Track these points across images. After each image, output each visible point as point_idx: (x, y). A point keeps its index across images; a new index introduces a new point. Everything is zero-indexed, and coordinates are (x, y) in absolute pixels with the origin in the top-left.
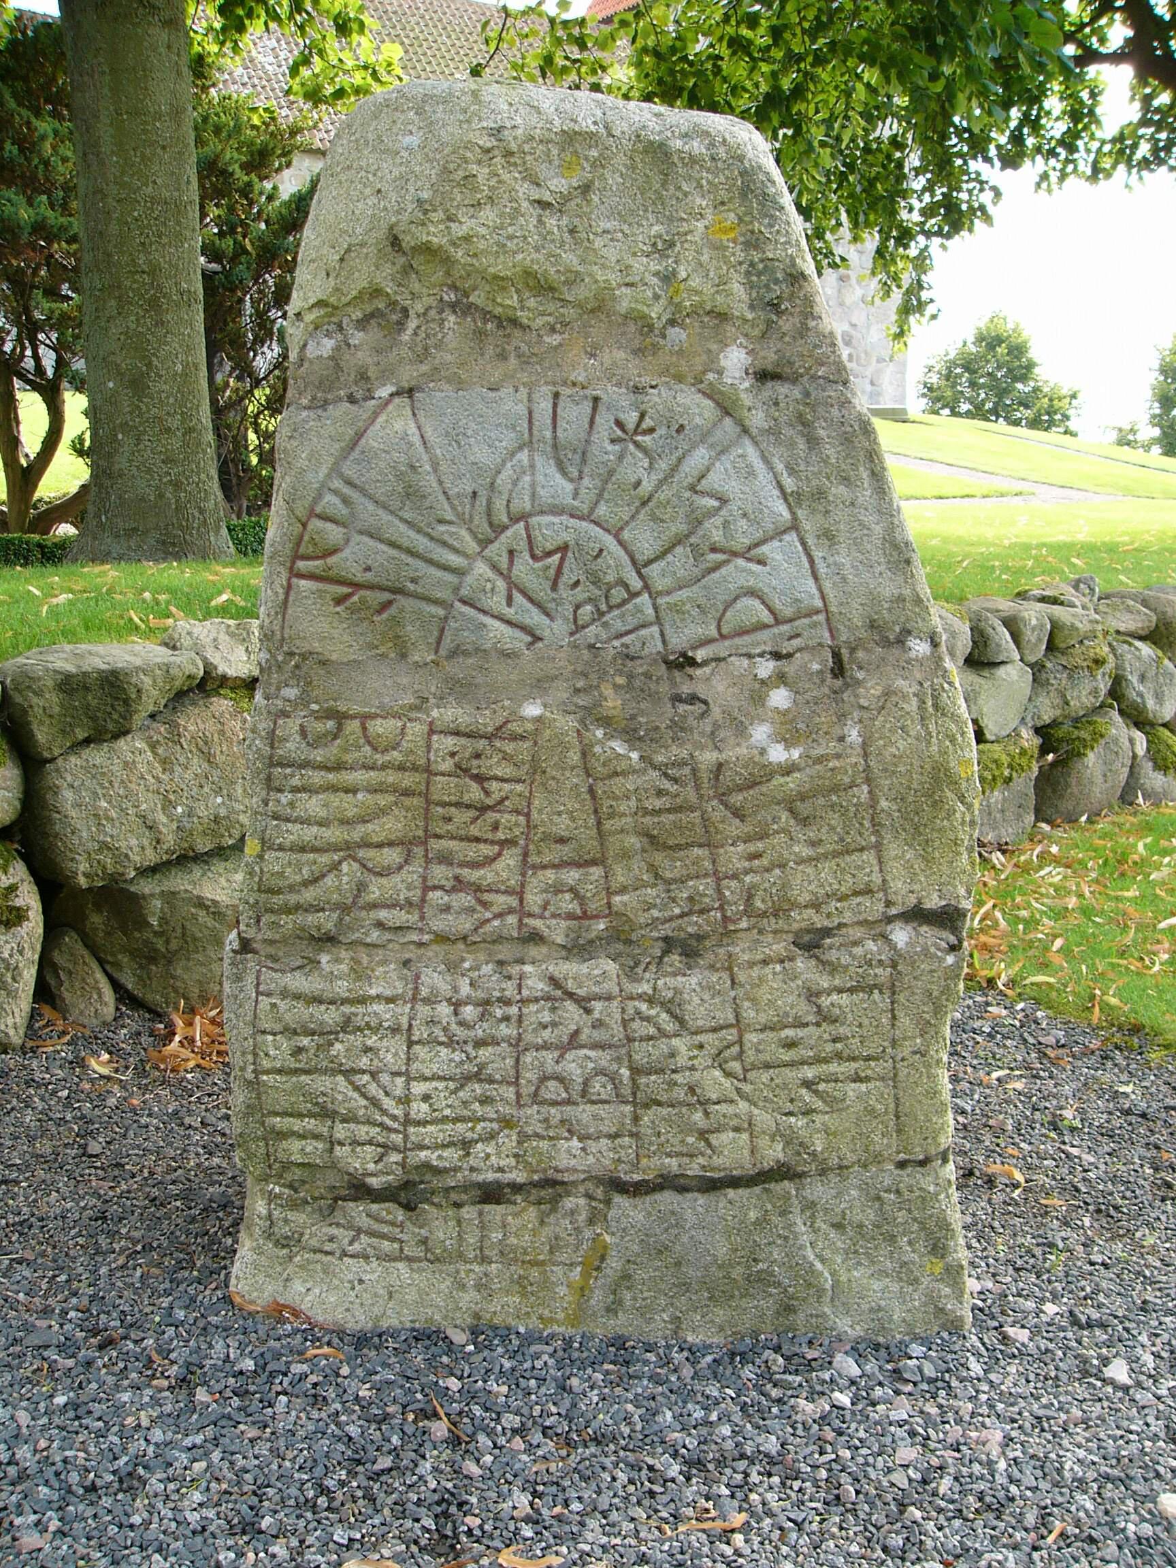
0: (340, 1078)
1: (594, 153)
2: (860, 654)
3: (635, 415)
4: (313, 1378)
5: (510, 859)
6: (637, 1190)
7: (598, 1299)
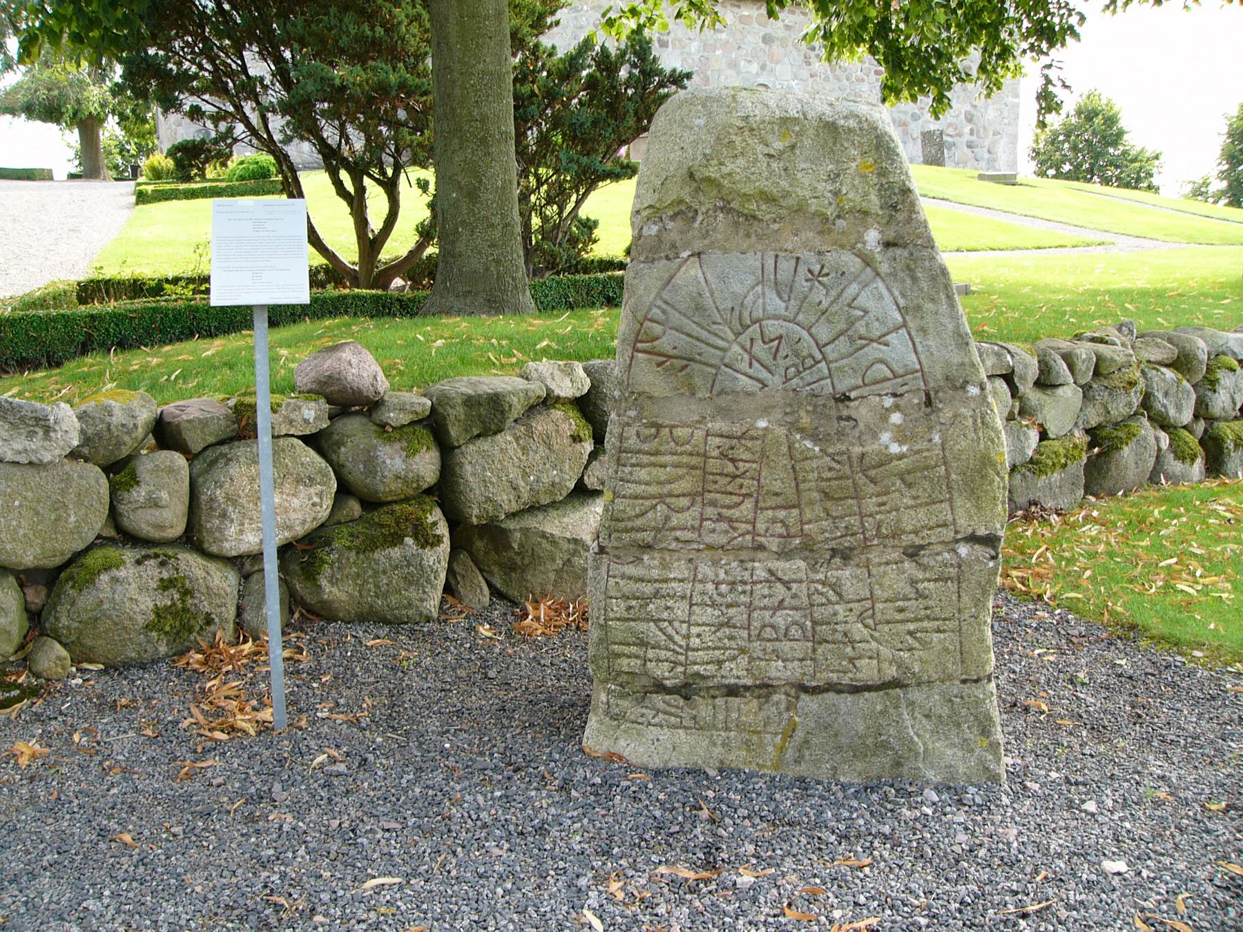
0: (652, 624)
1: (797, 128)
2: (940, 394)
3: (819, 267)
4: (633, 788)
5: (748, 505)
6: (815, 691)
7: (790, 754)
